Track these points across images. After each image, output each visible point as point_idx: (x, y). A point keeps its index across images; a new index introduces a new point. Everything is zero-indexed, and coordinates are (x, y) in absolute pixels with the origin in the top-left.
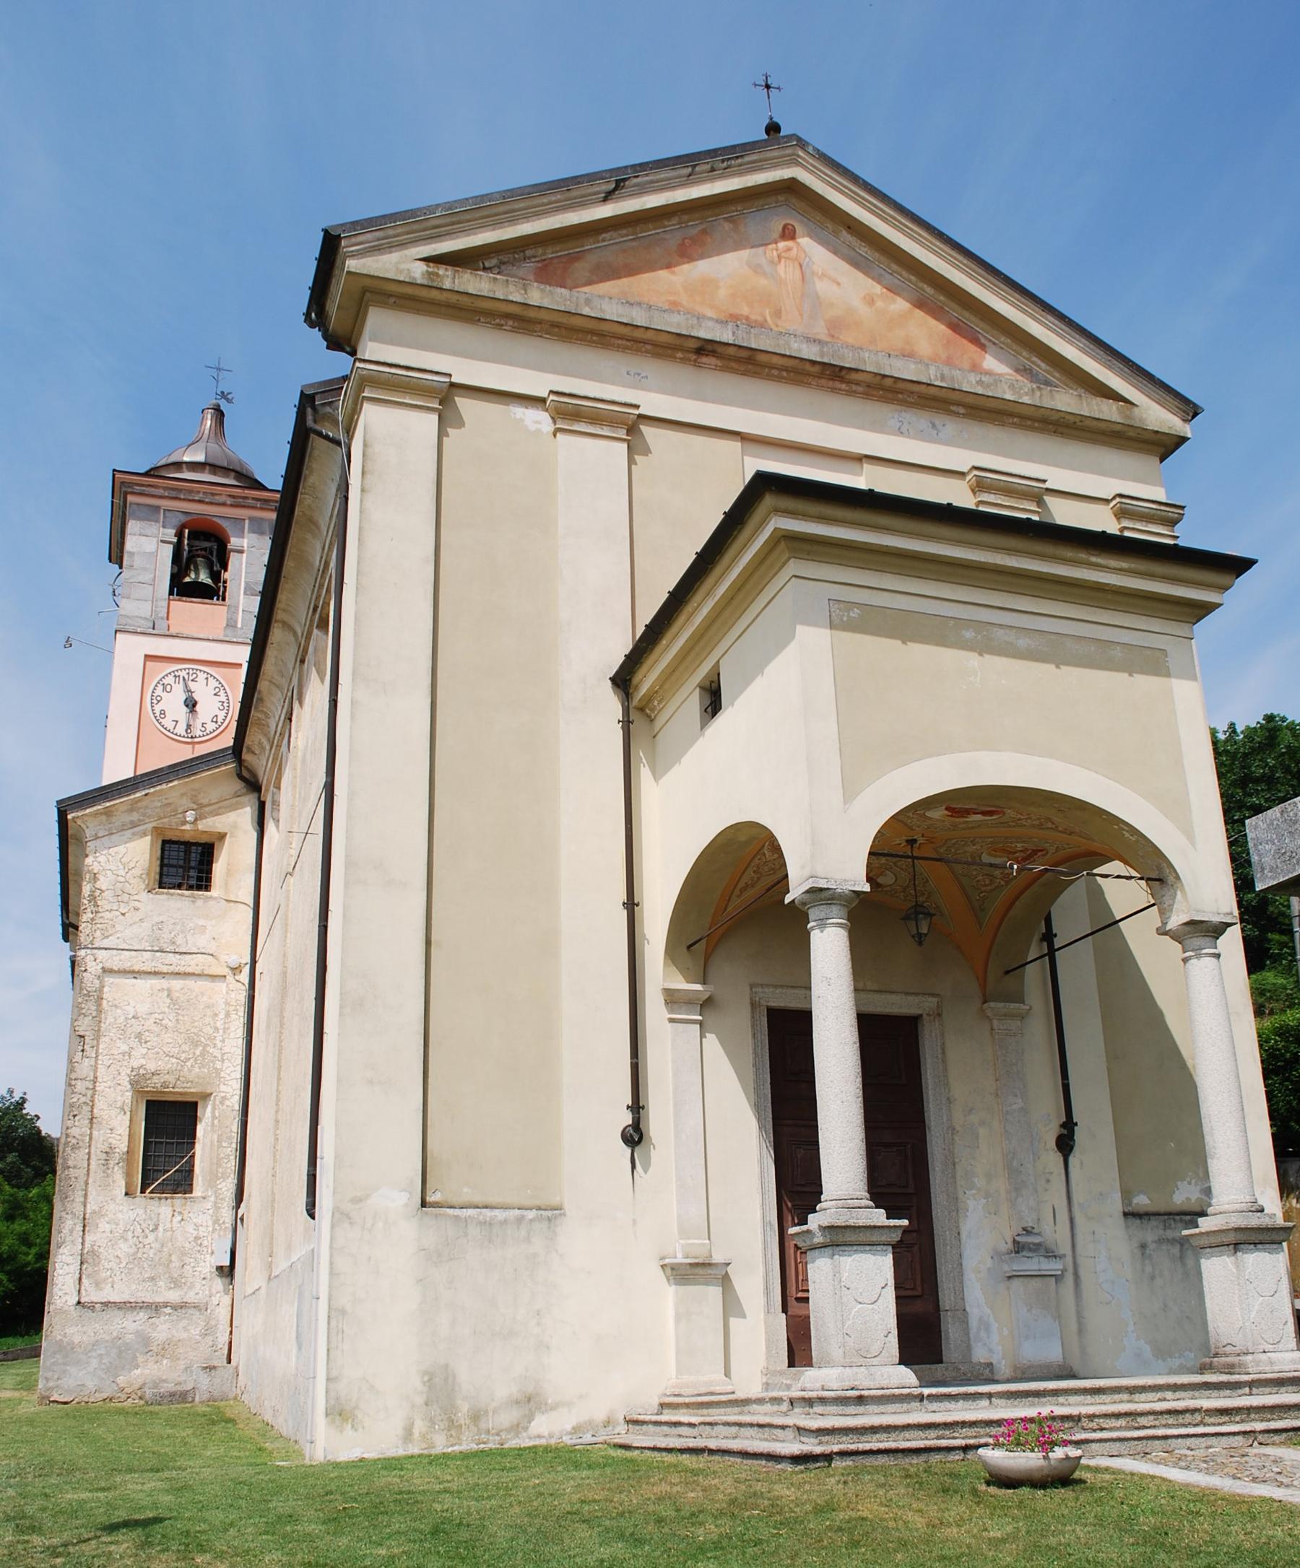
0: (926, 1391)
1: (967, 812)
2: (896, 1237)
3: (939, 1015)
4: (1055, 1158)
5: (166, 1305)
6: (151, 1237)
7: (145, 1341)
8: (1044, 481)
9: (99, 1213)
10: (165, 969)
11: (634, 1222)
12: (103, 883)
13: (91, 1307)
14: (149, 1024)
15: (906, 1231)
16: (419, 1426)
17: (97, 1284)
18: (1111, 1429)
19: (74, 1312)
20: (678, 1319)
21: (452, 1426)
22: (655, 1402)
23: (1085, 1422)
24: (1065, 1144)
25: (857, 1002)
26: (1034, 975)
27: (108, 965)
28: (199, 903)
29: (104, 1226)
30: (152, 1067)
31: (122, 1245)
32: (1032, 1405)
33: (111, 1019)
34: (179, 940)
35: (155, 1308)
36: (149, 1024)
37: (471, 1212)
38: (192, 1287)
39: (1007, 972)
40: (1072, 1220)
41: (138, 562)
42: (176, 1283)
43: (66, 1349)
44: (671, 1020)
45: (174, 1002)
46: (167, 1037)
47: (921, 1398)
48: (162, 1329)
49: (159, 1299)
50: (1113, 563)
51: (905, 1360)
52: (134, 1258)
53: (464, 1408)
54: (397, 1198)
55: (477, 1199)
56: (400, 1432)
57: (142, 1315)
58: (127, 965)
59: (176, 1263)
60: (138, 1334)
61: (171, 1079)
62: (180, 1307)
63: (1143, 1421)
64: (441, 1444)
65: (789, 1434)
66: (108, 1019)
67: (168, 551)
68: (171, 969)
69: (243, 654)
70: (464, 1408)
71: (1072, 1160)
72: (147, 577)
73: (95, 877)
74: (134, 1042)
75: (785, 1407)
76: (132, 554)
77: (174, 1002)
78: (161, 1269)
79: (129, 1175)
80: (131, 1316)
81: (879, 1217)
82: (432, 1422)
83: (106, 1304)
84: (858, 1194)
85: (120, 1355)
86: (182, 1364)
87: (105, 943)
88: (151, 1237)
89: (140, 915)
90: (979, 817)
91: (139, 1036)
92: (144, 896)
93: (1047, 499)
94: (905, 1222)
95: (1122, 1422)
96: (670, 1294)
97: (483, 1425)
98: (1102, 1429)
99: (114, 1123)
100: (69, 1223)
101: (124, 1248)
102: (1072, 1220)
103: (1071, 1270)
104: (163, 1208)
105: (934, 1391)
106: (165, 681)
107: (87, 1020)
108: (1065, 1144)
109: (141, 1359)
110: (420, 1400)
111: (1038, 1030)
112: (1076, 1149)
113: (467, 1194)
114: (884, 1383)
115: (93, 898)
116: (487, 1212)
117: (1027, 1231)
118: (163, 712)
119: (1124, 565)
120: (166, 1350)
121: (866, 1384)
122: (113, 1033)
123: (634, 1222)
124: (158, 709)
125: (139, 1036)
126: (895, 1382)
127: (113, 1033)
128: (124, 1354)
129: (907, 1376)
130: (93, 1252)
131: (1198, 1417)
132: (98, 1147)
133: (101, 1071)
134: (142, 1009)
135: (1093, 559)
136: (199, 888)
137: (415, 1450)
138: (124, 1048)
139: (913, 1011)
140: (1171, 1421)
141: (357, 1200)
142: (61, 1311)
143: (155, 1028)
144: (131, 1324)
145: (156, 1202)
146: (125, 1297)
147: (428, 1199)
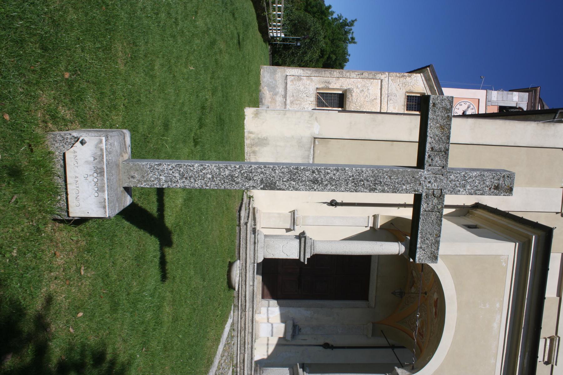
0: (256, 265)
1: (436, 306)
2: (302, 260)
3: (368, 307)
4: (322, 342)
5: (286, 100)
6: (305, 95)
7: (276, 94)
8: (556, 365)
9: (312, 80)
10: (382, 97)
11: (308, 202)
12: (408, 79)
13: (286, 79)
14: (366, 93)
15: (304, 263)
16: (252, 136)
17: (292, 81)
18: (241, 322)
19: (284, 74)
20: (279, 214)
21: (252, 145)
22: (255, 206)
23: (244, 313)
24: (326, 346)
25: (375, 256)
26: (382, 341)
27: (383, 81)
28: (403, 107)
29: (308, 82)
30: (354, 94)
31: (303, 87)
32: (249, 300)
33: (367, 82)
34: (391, 101)
35: (285, 97)
36: (366, 93)
37: (312, 152)
38: (291, 107)
39: (382, 331)
40: (302, 345)
41: (510, 96)
42: (292, 103)
43: (275, 72)
44: (369, 217)
45: (373, 100)
46: (362, 99)
47: (254, 263)
48: (279, 99)
49: (288, 98)
50: (526, 361)
51: (265, 260)
52: (299, 91)
53: (256, 149)
54: (317, 130)
55: (316, 155)
56: (251, 130)
57: (283, 93)
58: (383, 86)
59: (297, 102)
60: (278, 92)
61: (350, 100)
62: (285, 104)
63: (243, 333)
64: (247, 142)
65: (246, 220)
66: (367, 81)
67: (514, 105)
68: (383, 99)
69: (482, 111)
70: (256, 149)
71: (321, 348)
72: (505, 99)
73: (410, 76)
74: (361, 89)
75: (253, 227)
76: (512, 94)
77: (373, 100)
78: (296, 98)
79: (322, 89)
80: (283, 90)
81: (308, 256)
82: (253, 140)
83: (286, 83)
84: (315, 250)
85: (272, 87)
86: (269, 104)
87: (390, 80)
88: (305, 95)
89: (399, 90)
90: (434, 311)
91: (363, 91)
92: (404, 91)
93: (550, 365)
94: (306, 263)
95: (243, 325)
96: (286, 211)
97: (251, 154)
98: (241, 318)
99: (337, 84)
100: (309, 72)
101: (302, 88)
102: (302, 345)
103: (287, 343)
104: (313, 99)
105: (256, 267)
106: (471, 106)
107: (367, 75)
108: (326, 346)
109: (271, 93)
110: (259, 136)
111: (363, 341)
112: (324, 349)
113: (317, 152)
114: (259, 251)
115: (403, 76)
116: (312, 158)
117: (300, 330)
118: (461, 105)
119: (525, 365)
120: (273, 100)
121: (259, 246)
122: (363, 83)
123: (308, 202)
124: (462, 103)
125: (363, 91)
126: (259, 255)
127: (363, 83)
128: (273, 88)
129: (260, 260)
130: (301, 79)
131: (243, 352)
132: (330, 80)
133: (353, 80)
134: (370, 91)
135: (527, 354)
136: (407, 107)
137: (246, 134)
138: (359, 86)
139: (370, 299)
140: (242, 342)
141: (316, 119)
142: (285, 71)
143: (365, 95)
144: (281, 90)
145: (314, 96)
146: (288, 89)
147: (316, 140)
